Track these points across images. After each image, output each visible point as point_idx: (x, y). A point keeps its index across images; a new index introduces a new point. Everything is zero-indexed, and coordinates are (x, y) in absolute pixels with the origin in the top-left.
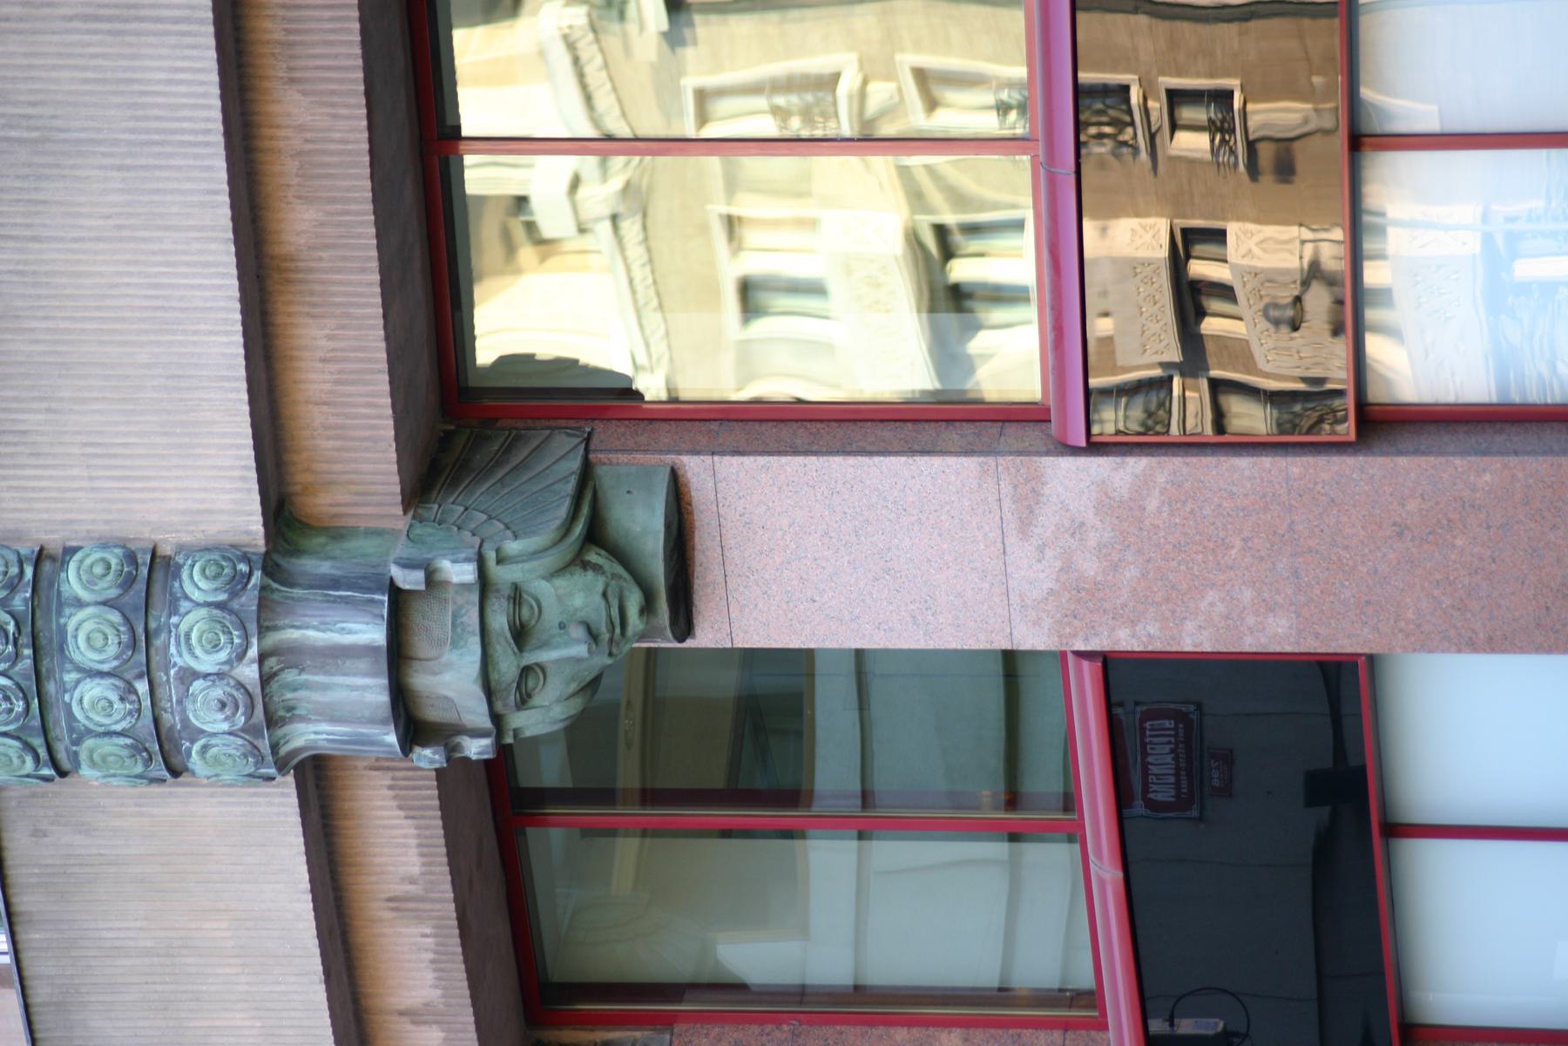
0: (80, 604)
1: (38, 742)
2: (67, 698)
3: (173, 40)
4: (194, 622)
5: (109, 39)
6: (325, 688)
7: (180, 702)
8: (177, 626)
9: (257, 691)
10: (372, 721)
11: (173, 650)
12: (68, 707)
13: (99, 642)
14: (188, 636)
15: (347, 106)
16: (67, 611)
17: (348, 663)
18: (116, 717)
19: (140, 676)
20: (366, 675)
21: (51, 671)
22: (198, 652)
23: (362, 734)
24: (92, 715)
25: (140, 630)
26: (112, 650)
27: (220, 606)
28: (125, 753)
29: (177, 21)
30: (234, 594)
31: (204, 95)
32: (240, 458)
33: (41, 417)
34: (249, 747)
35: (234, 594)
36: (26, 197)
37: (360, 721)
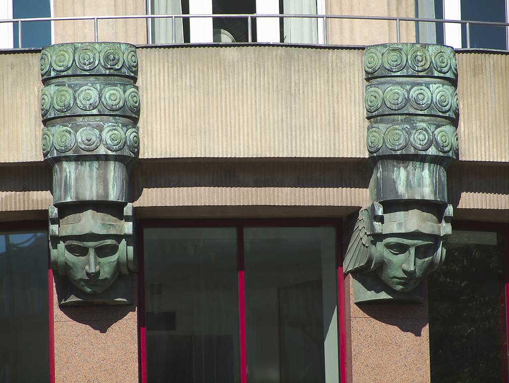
0: (124, 92)
1: (70, 72)
2: (89, 84)
3: (328, 142)
4: (120, 132)
5: (327, 121)
6: (91, 177)
7: (89, 125)
8: (118, 126)
9: (94, 153)
10: (77, 193)
11: (110, 124)
12: (86, 85)
13: (112, 98)
14: (116, 130)
15: (291, 199)
16: (122, 87)
17: (102, 186)
18: (83, 102)
19: (99, 111)
20: (97, 192)
21: (99, 80)
22: (110, 133)
23: (71, 189)
24: (83, 93)
25: (117, 113)
26: (110, 102)
27: (125, 142)
28: (66, 103)
29: (334, 144)
30: (129, 147)
31: (309, 152)
32: (175, 153)
33: (188, 83)
34: (70, 148)
35: (129, 147)
36: (270, 87)
37: (77, 188)
